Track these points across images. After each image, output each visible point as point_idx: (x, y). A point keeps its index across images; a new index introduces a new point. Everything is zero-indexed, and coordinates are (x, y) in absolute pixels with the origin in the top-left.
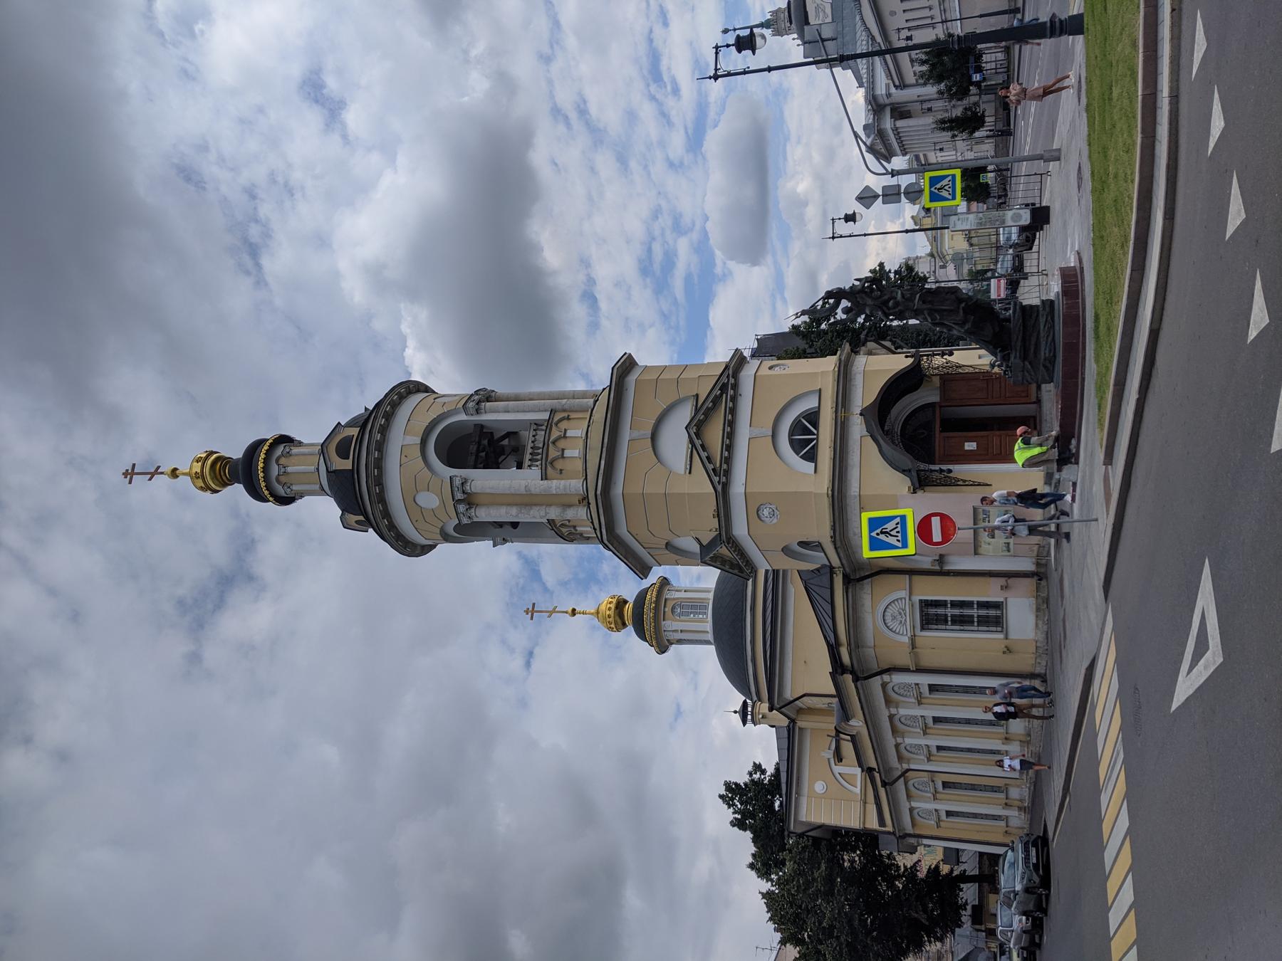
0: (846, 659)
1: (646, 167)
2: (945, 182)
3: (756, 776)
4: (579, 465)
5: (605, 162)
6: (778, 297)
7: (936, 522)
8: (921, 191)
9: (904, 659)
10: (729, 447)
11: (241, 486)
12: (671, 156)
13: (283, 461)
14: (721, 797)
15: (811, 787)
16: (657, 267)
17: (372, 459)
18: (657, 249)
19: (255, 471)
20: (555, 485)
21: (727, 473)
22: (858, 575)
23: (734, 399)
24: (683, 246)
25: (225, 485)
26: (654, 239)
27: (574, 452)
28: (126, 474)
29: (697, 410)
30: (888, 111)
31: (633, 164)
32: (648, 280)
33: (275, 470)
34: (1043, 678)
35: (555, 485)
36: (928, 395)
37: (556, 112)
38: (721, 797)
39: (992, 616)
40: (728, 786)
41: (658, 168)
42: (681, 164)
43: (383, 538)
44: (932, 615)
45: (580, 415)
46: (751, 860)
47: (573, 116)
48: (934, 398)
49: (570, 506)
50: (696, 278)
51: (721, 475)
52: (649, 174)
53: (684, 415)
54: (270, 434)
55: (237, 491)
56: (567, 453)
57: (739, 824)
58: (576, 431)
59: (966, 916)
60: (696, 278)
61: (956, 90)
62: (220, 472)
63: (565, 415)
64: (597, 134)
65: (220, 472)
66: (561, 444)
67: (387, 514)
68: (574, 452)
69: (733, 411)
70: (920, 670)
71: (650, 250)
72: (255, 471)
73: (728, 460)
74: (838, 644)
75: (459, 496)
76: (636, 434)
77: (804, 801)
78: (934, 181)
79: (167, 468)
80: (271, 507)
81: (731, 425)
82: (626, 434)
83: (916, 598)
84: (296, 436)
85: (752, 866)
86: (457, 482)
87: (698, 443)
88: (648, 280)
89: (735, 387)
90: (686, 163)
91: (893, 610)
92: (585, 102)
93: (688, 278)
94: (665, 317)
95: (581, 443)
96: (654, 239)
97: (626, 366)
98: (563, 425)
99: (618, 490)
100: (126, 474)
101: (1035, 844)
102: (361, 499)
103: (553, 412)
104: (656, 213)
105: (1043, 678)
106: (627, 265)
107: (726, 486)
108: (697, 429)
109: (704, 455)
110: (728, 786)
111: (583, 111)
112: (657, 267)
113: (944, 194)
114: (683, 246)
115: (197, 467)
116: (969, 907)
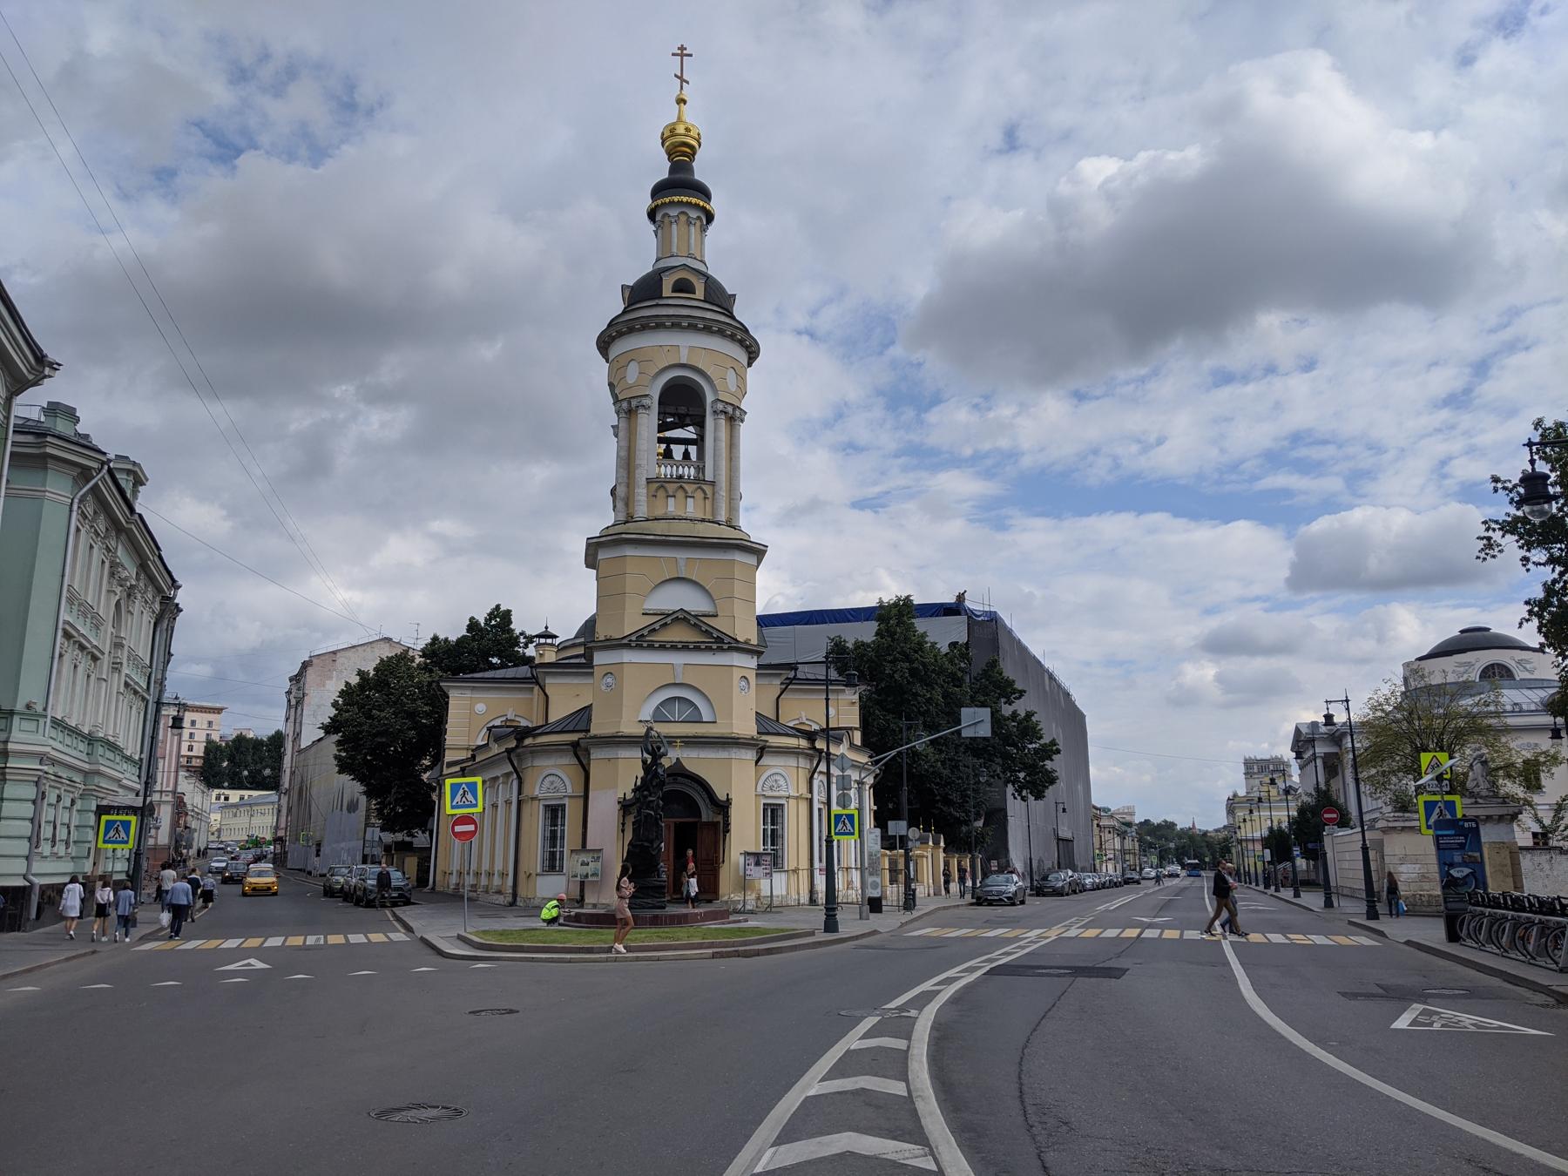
0: (528, 741)
1: (1438, 430)
2: (123, 834)
3: (522, 640)
4: (659, 512)
5: (1444, 380)
6: (1267, 605)
7: (471, 828)
8: (844, 807)
9: (527, 791)
10: (663, 647)
11: (666, 175)
12: (1456, 462)
13: (683, 218)
14: (498, 607)
15: (480, 700)
16: (1303, 452)
17: (663, 320)
18: (1328, 452)
19: (680, 191)
20: (641, 492)
21: (639, 647)
22: (580, 752)
23: (709, 649)
24: (1332, 484)
25: (669, 155)
26: (1340, 446)
27: (672, 507)
28: (682, 48)
29: (695, 616)
30: (1334, 750)
31: (1444, 414)
32: (1286, 443)
33: (673, 212)
34: (513, 903)
35: (641, 492)
36: (707, 815)
37: (1514, 313)
38: (498, 607)
39: (553, 864)
40: (508, 612)
41: (1439, 447)
42: (1445, 476)
43: (609, 325)
44: (555, 813)
45: (708, 508)
46: (442, 637)
47: (1507, 335)
48: (704, 819)
49: (627, 505)
50: (1288, 503)
51: (639, 641)
52: (1430, 435)
53: (692, 602)
54: (715, 205)
55: (662, 171)
56: (671, 501)
57: (473, 625)
58: (692, 508)
59: (399, 837)
60: (1288, 503)
61: (1393, 819)
62: (681, 152)
63: (709, 494)
64: (1481, 368)
65: (681, 152)
66: (680, 494)
67: (631, 330)
68: (672, 507)
69: (697, 648)
70: (519, 803)
71: (1325, 442)
72: (680, 191)
73: (651, 647)
74: (535, 736)
75: (634, 403)
76: (682, 563)
77: (468, 694)
78: (850, 817)
79: (686, 95)
80: (647, 202)
81: (685, 647)
82: (682, 555)
83: (566, 801)
84: (711, 228)
85: (435, 639)
86: (646, 401)
87: (669, 620)
88: (1286, 443)
89: (720, 649)
90: (1447, 482)
91: (558, 783)
92: (1527, 349)
93: (1287, 493)
94: (1234, 467)
95: (681, 513)
96: (1340, 446)
97: (758, 552)
98: (699, 495)
99: (630, 551)
100: (682, 48)
101: (400, 896)
102: (647, 302)
103: (713, 483)
104: (1376, 448)
105: (513, 903)
106: (1300, 417)
107: (628, 646)
108: (682, 618)
109: (657, 626)
110: (508, 612)
111: (1512, 347)
112: (1303, 452)
113: (112, 833)
114: (1332, 484)
115: (681, 129)
116: (408, 839)
